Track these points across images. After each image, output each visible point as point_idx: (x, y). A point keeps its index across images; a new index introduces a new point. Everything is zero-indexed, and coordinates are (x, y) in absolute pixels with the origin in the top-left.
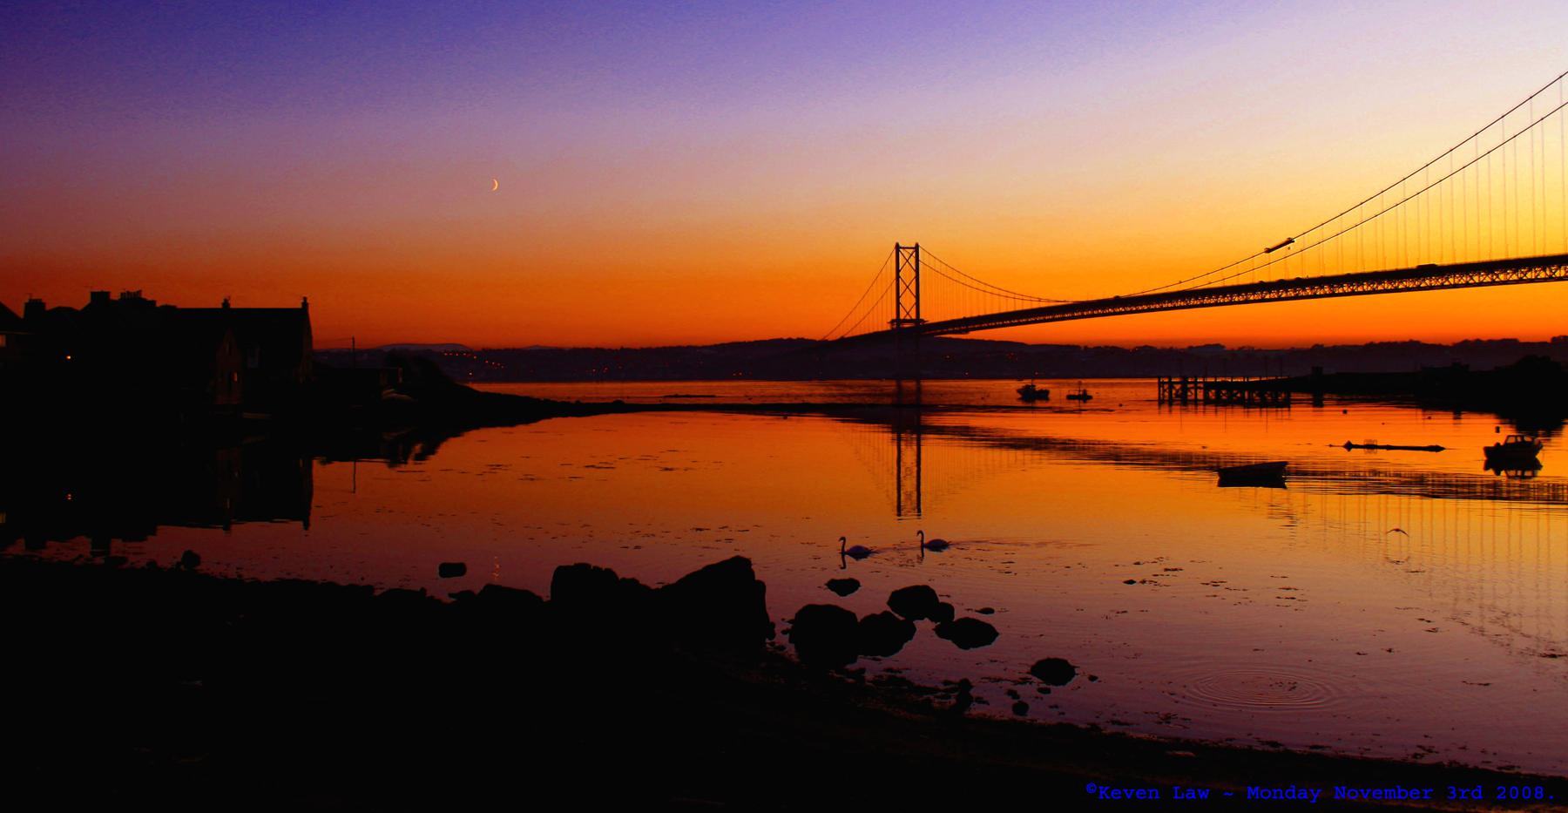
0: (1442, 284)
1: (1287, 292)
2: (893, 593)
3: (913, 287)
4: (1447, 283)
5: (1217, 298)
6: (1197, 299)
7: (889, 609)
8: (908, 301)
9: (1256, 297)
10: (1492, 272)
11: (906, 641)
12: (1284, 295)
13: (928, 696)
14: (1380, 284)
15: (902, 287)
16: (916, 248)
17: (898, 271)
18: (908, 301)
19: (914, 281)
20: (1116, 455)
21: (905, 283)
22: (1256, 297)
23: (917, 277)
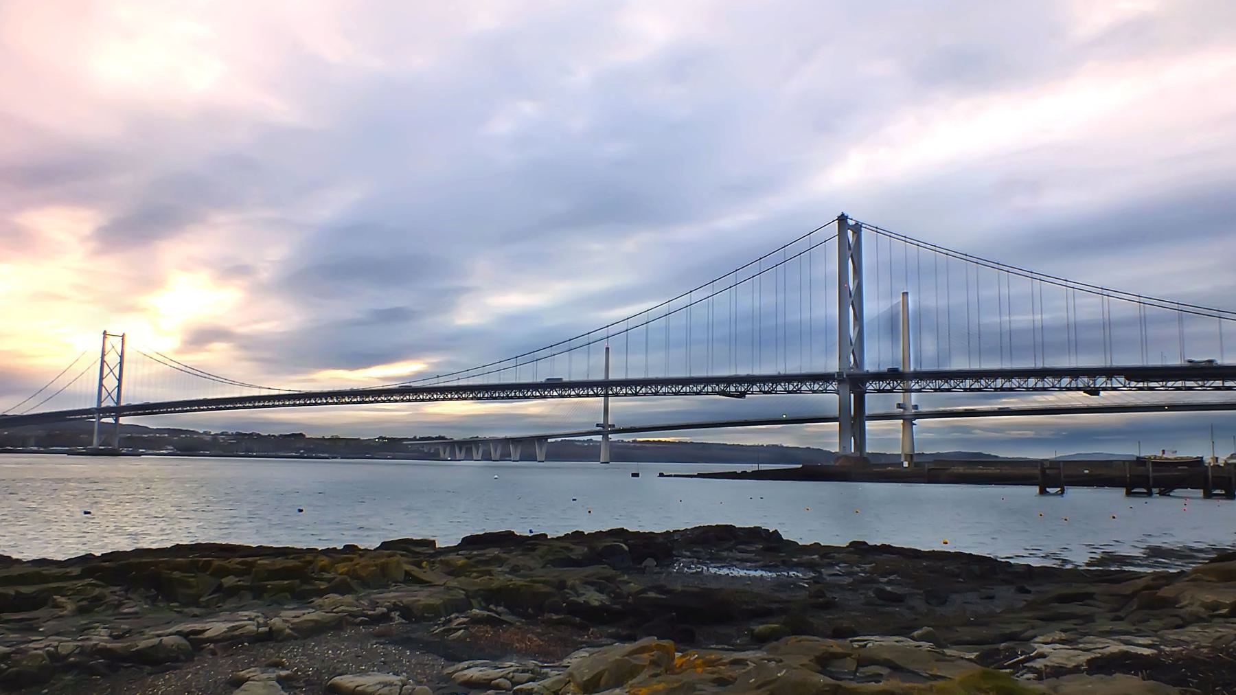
0: (430, 398)
1: (321, 399)
2: (463, 539)
3: (117, 372)
4: (418, 398)
5: (274, 402)
6: (250, 403)
7: (983, 668)
8: (110, 383)
9: (291, 403)
10: (430, 394)
11: (459, 544)
12: (319, 402)
13: (533, 636)
14: (392, 396)
15: (106, 370)
16: (123, 336)
17: (101, 379)
18: (110, 383)
19: (116, 389)
20: (708, 346)
21: (112, 398)
22: (291, 403)
23: (121, 363)
